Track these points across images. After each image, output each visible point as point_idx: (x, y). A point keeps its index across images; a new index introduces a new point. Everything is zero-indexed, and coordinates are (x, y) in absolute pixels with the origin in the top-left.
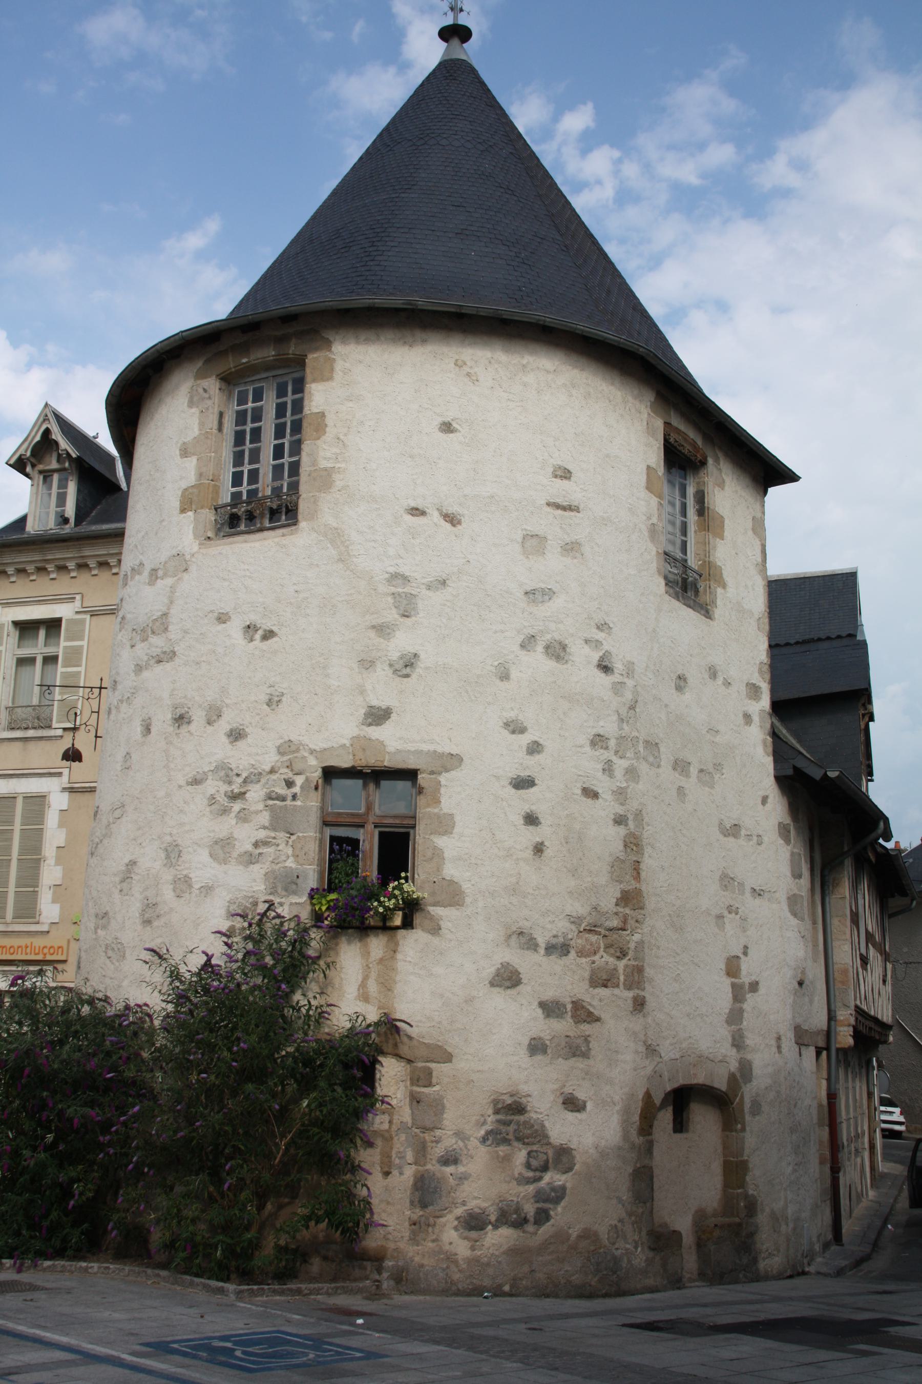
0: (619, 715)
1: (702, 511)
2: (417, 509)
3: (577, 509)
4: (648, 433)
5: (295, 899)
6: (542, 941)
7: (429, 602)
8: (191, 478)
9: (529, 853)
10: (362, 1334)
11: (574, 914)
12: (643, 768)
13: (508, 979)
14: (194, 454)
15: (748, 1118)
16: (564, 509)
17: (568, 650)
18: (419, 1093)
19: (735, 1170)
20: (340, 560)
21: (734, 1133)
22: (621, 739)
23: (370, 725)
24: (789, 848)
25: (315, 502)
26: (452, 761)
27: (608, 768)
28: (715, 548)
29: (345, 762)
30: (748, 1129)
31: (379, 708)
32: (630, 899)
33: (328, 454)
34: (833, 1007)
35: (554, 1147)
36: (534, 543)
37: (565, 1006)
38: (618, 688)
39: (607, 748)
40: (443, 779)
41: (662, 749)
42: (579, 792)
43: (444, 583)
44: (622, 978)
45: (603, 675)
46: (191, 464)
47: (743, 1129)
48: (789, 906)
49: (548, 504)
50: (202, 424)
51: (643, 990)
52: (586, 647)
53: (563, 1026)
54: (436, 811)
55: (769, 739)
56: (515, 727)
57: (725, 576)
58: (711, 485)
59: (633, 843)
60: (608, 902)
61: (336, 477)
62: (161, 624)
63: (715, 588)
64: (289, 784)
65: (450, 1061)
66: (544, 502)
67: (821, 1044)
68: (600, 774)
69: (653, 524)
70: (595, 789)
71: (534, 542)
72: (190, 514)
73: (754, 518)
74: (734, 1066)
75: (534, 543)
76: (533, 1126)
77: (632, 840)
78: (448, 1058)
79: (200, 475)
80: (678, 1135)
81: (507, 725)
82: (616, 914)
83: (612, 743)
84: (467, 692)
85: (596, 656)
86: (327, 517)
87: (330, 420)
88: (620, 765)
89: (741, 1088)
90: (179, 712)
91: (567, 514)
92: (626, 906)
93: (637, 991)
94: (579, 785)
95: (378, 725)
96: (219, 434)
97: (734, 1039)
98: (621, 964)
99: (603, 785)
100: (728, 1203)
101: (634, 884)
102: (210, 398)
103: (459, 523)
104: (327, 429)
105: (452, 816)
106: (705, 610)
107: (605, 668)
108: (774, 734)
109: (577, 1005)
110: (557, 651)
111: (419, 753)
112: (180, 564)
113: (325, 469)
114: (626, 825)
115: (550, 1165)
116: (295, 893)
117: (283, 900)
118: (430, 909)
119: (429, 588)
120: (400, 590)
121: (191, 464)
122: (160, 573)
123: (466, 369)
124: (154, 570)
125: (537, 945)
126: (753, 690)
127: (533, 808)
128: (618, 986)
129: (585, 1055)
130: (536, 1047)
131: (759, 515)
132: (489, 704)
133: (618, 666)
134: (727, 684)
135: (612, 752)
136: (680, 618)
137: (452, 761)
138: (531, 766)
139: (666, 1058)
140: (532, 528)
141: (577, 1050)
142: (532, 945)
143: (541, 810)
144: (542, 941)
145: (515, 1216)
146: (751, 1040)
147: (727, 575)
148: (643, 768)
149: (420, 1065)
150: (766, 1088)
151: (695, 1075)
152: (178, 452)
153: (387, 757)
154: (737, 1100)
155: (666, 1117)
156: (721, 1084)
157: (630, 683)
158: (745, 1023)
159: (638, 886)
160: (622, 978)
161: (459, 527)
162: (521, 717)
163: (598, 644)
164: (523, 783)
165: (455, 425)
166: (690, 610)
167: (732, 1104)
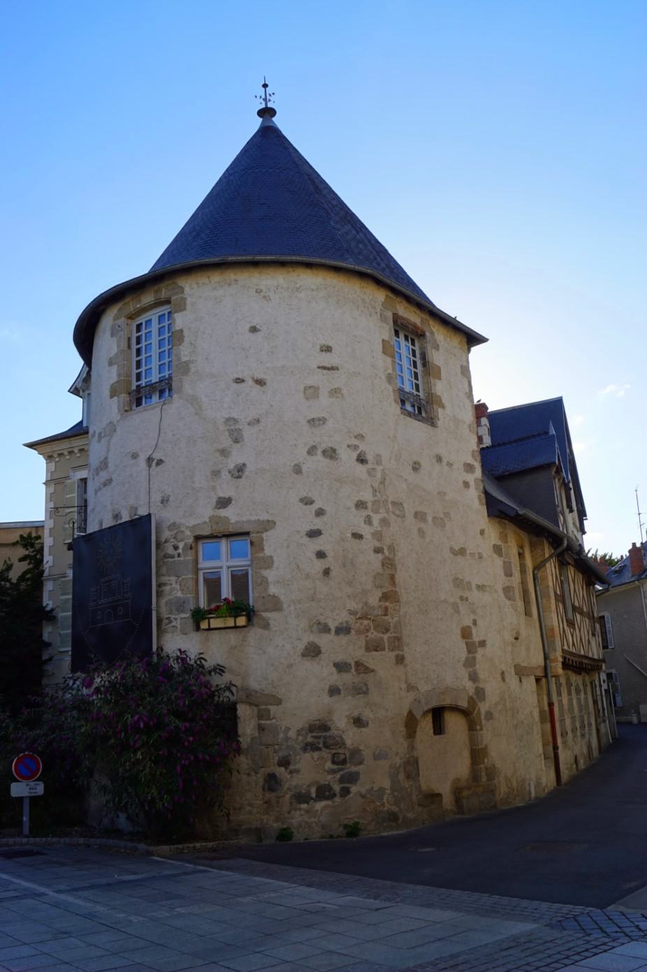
0: (373, 488)
1: (425, 363)
2: (239, 379)
3: (337, 369)
4: (382, 320)
5: (183, 615)
6: (332, 626)
7: (248, 433)
8: (114, 378)
9: (321, 575)
10: (206, 871)
11: (352, 609)
12: (392, 518)
13: (313, 651)
14: (115, 364)
15: (484, 722)
16: (329, 369)
17: (337, 452)
18: (264, 724)
19: (477, 754)
20: (197, 414)
21: (476, 732)
22: (374, 503)
23: (220, 508)
24: (502, 558)
25: (181, 382)
26: (269, 525)
27: (368, 521)
28: (435, 385)
29: (206, 531)
30: (484, 728)
31: (224, 498)
32: (389, 597)
33: (186, 353)
34: (547, 652)
35: (349, 749)
36: (312, 392)
37: (350, 665)
38: (371, 473)
39: (366, 508)
40: (264, 535)
41: (405, 506)
42: (350, 535)
43: (258, 421)
44: (387, 644)
45: (361, 465)
46: (115, 368)
47: (481, 729)
48: (504, 593)
49: (319, 367)
50: (118, 346)
51: (403, 650)
52: (348, 449)
53: (349, 678)
54: (262, 555)
55: (483, 496)
56: (308, 502)
57: (443, 401)
58: (429, 348)
59: (389, 563)
60: (374, 600)
61: (191, 366)
62: (104, 464)
63: (437, 409)
64: (176, 548)
65: (281, 704)
66: (316, 366)
67: (540, 673)
68: (362, 524)
69: (389, 374)
70: (360, 533)
71: (310, 391)
72: (116, 398)
73: (462, 366)
74: (471, 692)
75: (312, 392)
76: (334, 738)
77: (387, 561)
78: (279, 702)
79: (119, 375)
80: (437, 737)
81: (301, 500)
82: (380, 606)
83: (369, 505)
84: (276, 483)
85: (355, 455)
86: (188, 389)
87: (186, 333)
88: (376, 519)
89: (477, 705)
90: (116, 512)
91: (330, 372)
92: (386, 601)
93: (397, 652)
94: (349, 532)
95: (224, 508)
96: (129, 351)
97: (470, 675)
98: (386, 637)
99: (366, 530)
100: (475, 776)
101: (390, 588)
102: (122, 330)
103: (265, 384)
104: (185, 339)
105: (271, 557)
106: (431, 421)
107: (362, 460)
108: (486, 493)
109: (358, 664)
110: (331, 454)
111: (249, 522)
112: (112, 428)
113: (185, 362)
114: (383, 553)
115: (348, 761)
116: (183, 612)
117: (176, 617)
118: (264, 614)
119: (249, 424)
120: (233, 427)
121: (115, 368)
122: (103, 435)
123: (263, 294)
124: (100, 433)
125: (330, 630)
126: (469, 468)
127: (322, 548)
128: (384, 649)
129: (366, 693)
130: (334, 691)
131: (465, 364)
132: (290, 488)
133: (369, 457)
134: (450, 465)
135: (370, 510)
136: (417, 429)
137: (269, 525)
138: (318, 524)
139: (422, 691)
140: (310, 383)
141: (360, 690)
142: (325, 629)
143: (327, 548)
144: (332, 626)
145: (327, 793)
146: (482, 675)
147: (445, 400)
148: (392, 518)
149: (262, 707)
150: (496, 704)
151: (444, 699)
152: (107, 364)
153: (231, 526)
154: (476, 712)
155: (426, 725)
156: (464, 704)
157: (380, 468)
158: (477, 666)
159: (394, 589)
160: (387, 644)
161: (265, 386)
162: (310, 495)
163: (356, 447)
164: (314, 534)
165: (258, 327)
166: (420, 423)
167: (472, 714)
